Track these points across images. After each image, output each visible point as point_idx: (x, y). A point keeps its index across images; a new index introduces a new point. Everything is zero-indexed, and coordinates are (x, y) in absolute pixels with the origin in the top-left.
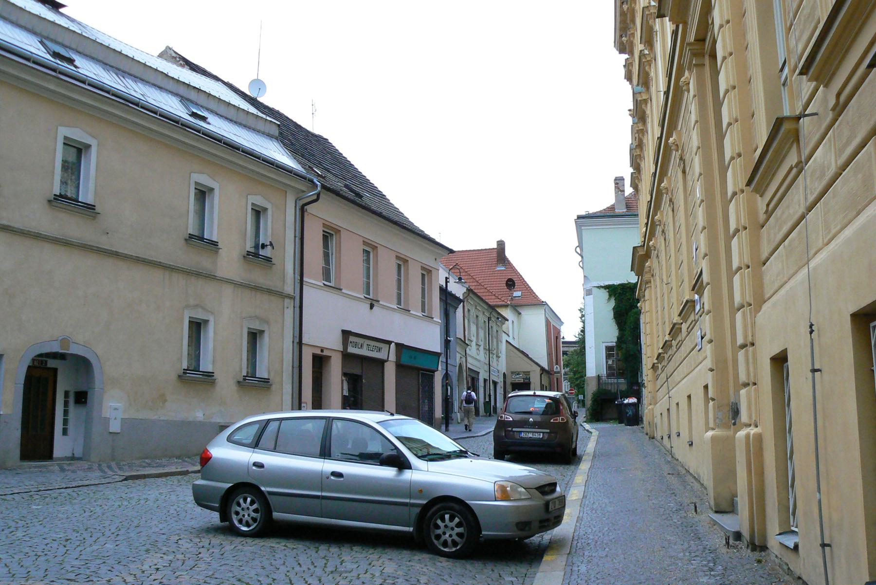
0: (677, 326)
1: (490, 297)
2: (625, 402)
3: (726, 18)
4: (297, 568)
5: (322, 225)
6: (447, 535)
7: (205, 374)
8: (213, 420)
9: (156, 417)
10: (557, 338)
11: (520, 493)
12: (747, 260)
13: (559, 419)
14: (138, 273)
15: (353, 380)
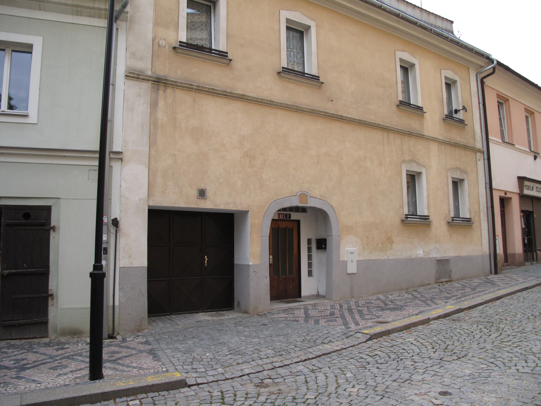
5: (496, 96)
7: (422, 217)
8: (431, 256)
9: (385, 257)
14: (361, 134)
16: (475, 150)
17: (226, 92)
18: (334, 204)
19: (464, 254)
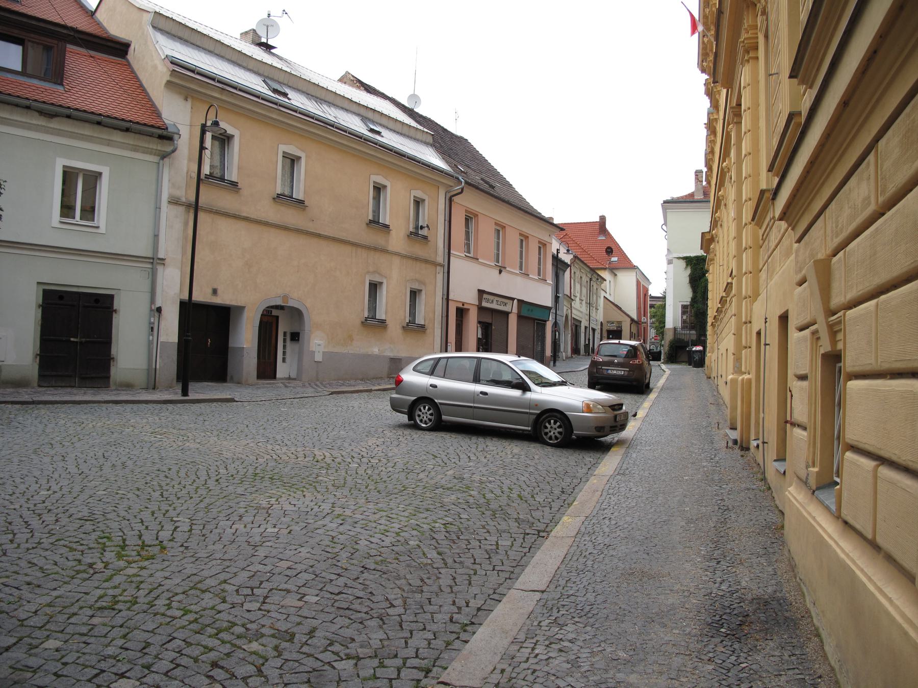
0: (724, 299)
1: (592, 262)
2: (693, 349)
3: (748, 106)
4: (460, 448)
6: (552, 433)
8: (385, 354)
9: (346, 351)
10: (645, 295)
11: (599, 409)
12: (750, 269)
13: (637, 362)
14: (335, 249)
15: (486, 327)
16: (435, 264)
17: (236, 215)
18: (308, 305)
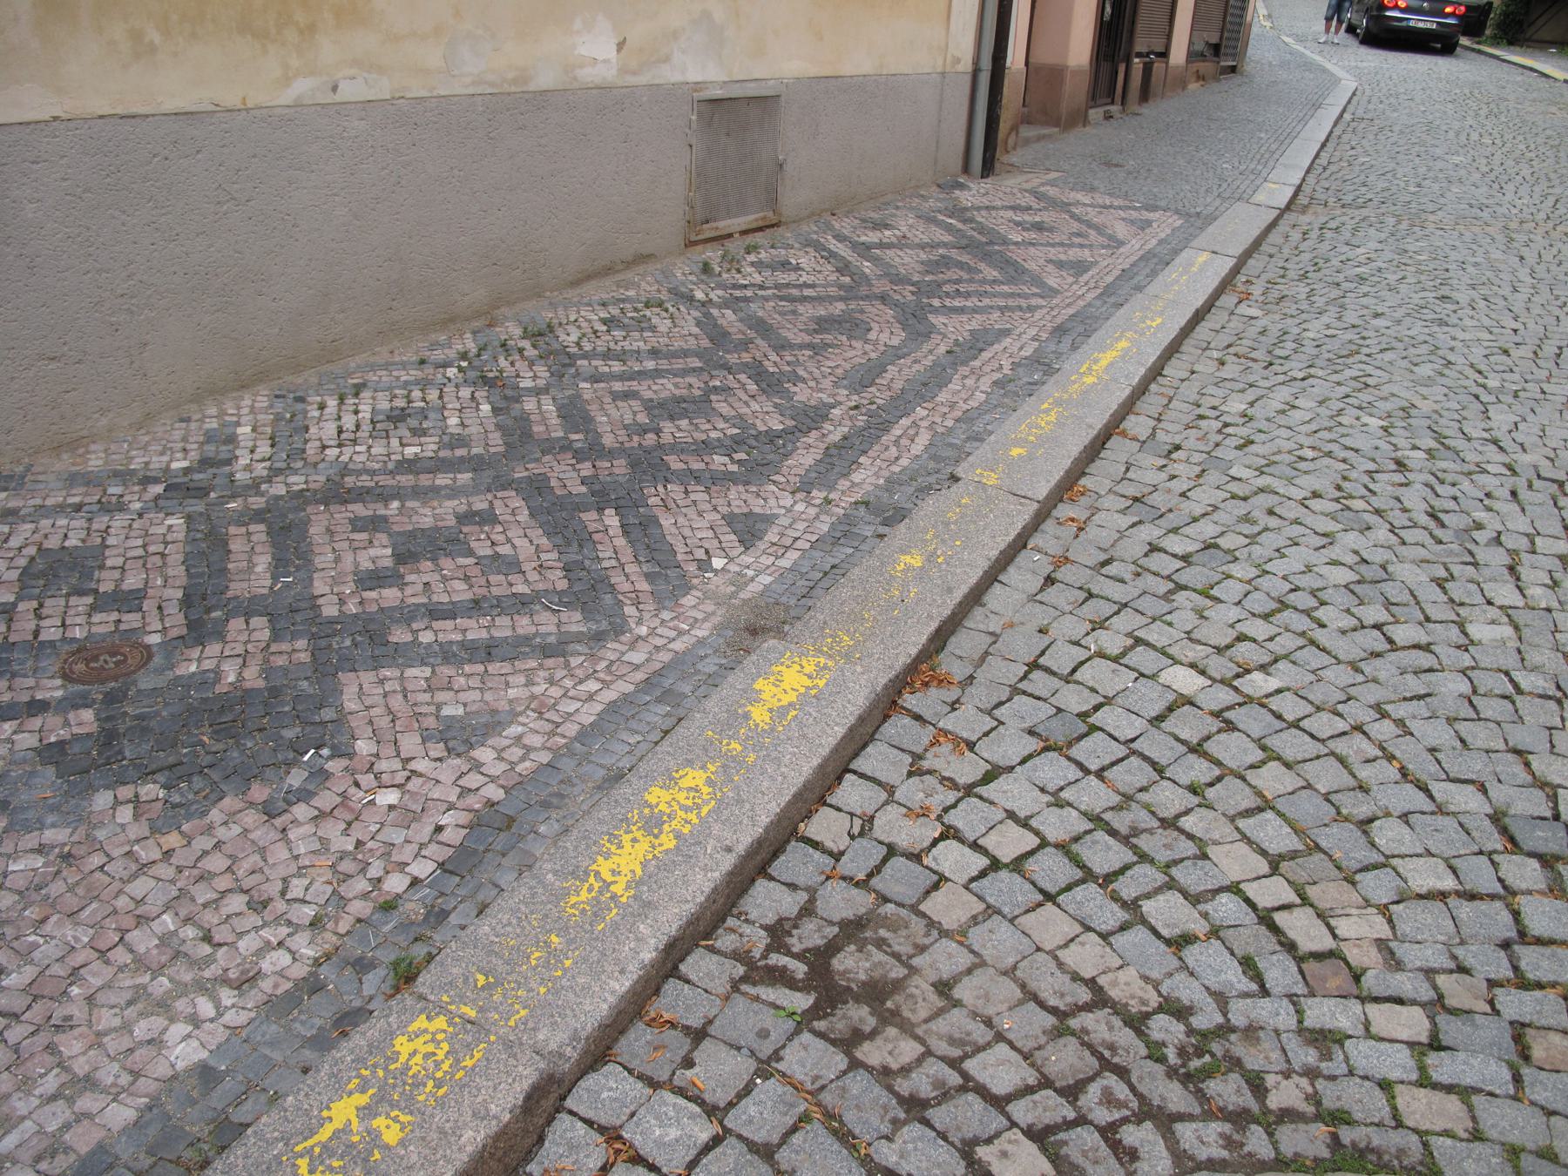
8: (669, 75)
9: (302, 87)
19: (858, 63)
